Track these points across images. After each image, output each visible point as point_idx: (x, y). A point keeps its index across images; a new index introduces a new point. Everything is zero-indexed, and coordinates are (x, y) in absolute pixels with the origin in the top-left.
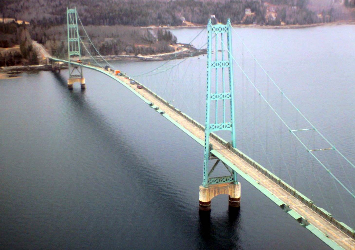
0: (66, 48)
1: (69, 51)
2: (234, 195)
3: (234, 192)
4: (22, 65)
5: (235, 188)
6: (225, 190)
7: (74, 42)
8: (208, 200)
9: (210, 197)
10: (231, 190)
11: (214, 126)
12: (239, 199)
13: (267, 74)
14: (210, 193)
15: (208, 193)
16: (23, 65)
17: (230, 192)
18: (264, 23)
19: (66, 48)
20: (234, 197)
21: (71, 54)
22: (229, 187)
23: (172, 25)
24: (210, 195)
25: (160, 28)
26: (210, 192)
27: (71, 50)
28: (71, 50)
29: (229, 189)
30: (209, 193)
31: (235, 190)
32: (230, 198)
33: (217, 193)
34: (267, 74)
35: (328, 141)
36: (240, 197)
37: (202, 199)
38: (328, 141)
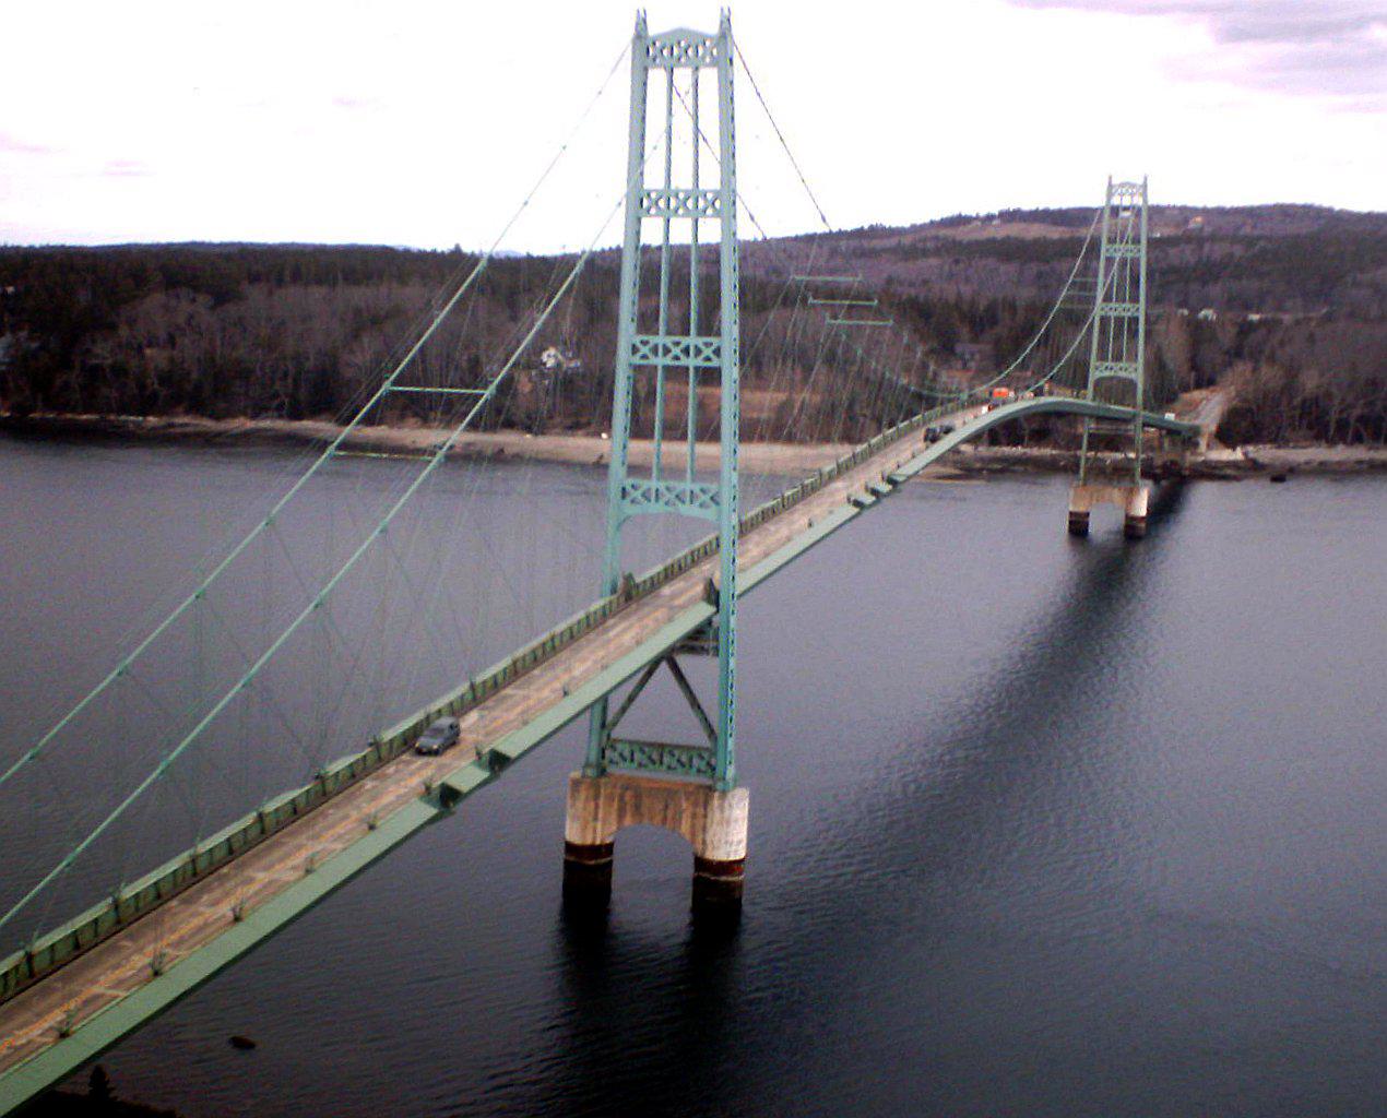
2: (704, 842)
3: (704, 829)
6: (667, 807)
7: (1120, 321)
8: (584, 837)
9: (599, 826)
13: (851, 323)
14: (597, 806)
15: (587, 800)
17: (689, 823)
18: (1193, 440)
20: (704, 850)
21: (1098, 374)
23: (1199, 386)
24: (600, 816)
27: (1102, 357)
29: (684, 805)
30: (592, 804)
32: (701, 863)
33: (633, 816)
34: (851, 323)
35: (447, 309)
37: (573, 834)
38: (447, 309)
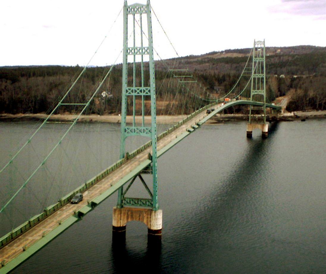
0: (267, 86)
1: (252, 90)
2: (150, 225)
3: (150, 221)
4: (242, 114)
5: (151, 216)
9: (122, 221)
10: (147, 218)
11: (137, 132)
12: (159, 231)
15: (118, 214)
16: (242, 113)
19: (267, 86)
20: (151, 227)
22: (144, 213)
24: (122, 218)
25: (273, 106)
26: (121, 214)
28: (254, 89)
29: (145, 215)
31: (151, 219)
36: (161, 230)
37: (115, 224)
